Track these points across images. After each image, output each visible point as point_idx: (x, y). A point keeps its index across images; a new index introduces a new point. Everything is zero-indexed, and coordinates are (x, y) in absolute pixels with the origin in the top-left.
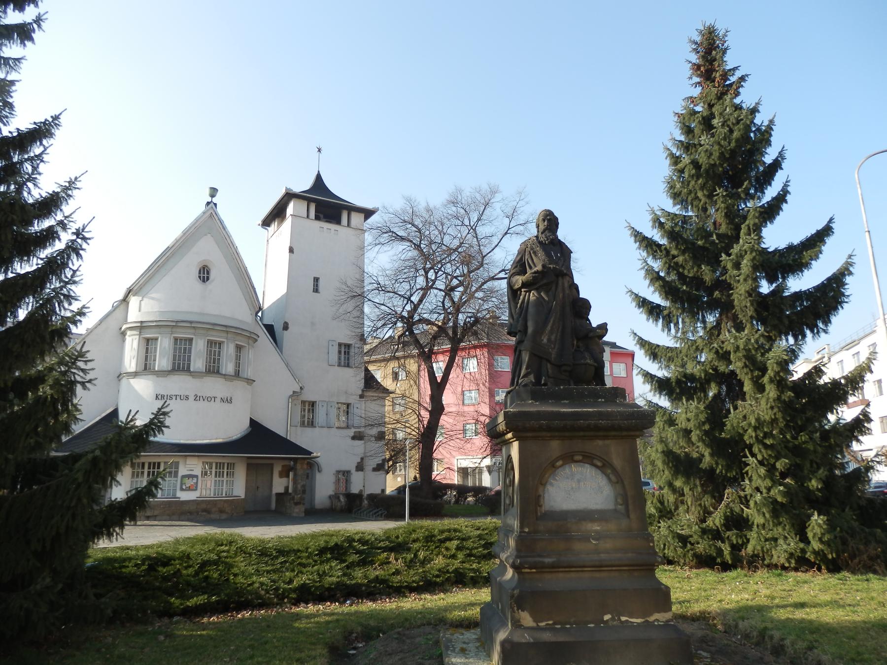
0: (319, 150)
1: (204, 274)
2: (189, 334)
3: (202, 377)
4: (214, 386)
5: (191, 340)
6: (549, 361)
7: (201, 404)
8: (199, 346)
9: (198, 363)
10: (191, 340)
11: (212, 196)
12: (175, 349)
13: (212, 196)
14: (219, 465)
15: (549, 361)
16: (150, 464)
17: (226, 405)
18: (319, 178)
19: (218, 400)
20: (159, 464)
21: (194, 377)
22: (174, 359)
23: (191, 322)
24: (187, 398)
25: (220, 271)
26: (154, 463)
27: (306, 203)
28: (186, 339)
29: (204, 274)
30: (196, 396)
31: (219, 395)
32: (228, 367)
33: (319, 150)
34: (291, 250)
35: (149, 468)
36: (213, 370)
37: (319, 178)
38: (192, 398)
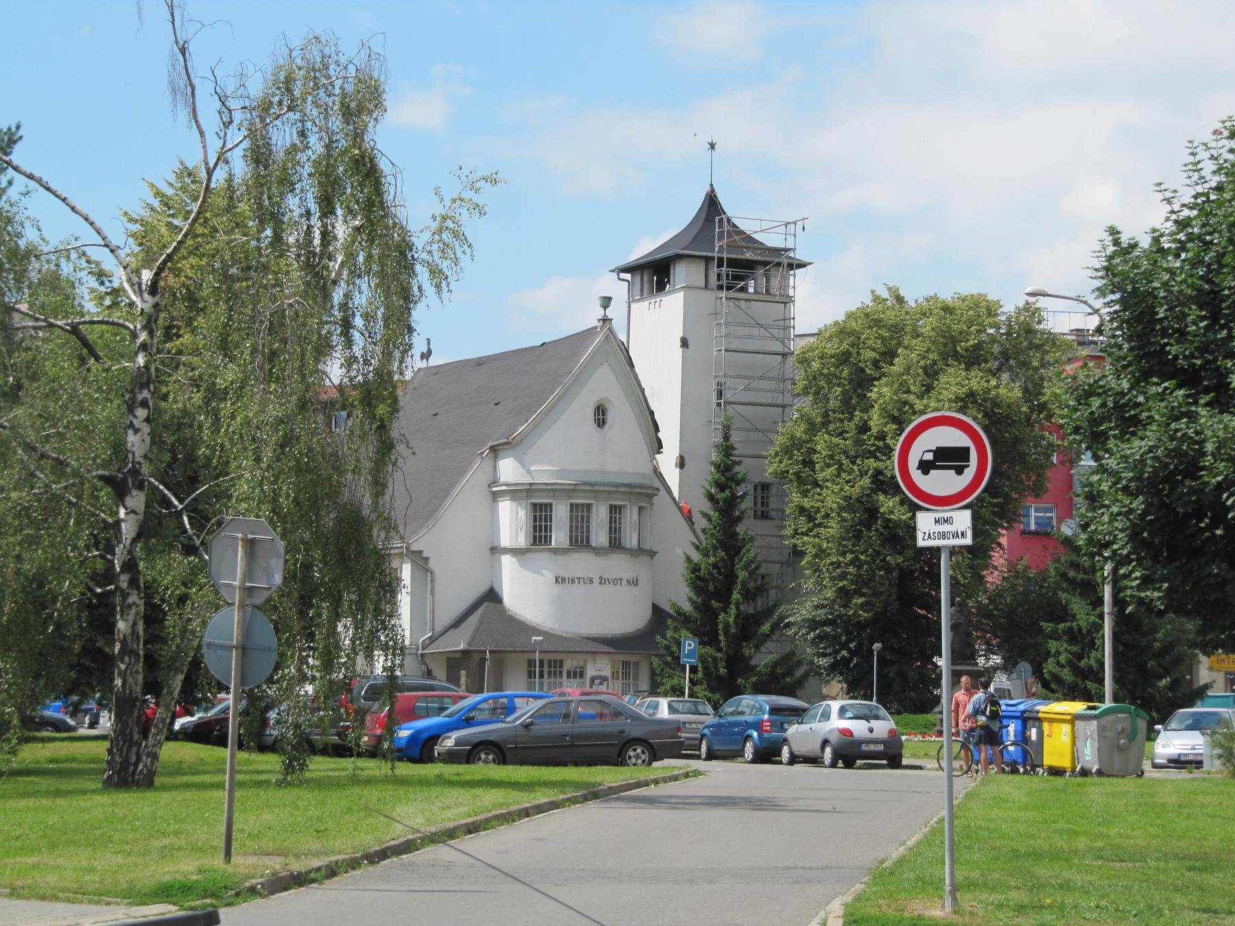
0: (712, 146)
1: (601, 415)
2: (547, 497)
3: (528, 555)
4: (619, 565)
5: (589, 506)
6: (515, 552)
7: (607, 588)
8: (561, 513)
9: (600, 537)
10: (589, 506)
11: (605, 307)
12: (571, 517)
13: (605, 307)
14: (626, 665)
15: (515, 552)
16: (550, 662)
17: (632, 588)
18: (712, 205)
19: (624, 582)
20: (561, 662)
21: (597, 554)
22: (571, 531)
23: (592, 485)
24: (591, 581)
25: (622, 416)
26: (555, 661)
27: (703, 264)
28: (583, 505)
29: (601, 415)
30: (601, 578)
31: (626, 576)
32: (631, 540)
33: (712, 146)
34: (684, 343)
35: (549, 666)
36: (615, 544)
37: (712, 205)
38: (596, 581)
